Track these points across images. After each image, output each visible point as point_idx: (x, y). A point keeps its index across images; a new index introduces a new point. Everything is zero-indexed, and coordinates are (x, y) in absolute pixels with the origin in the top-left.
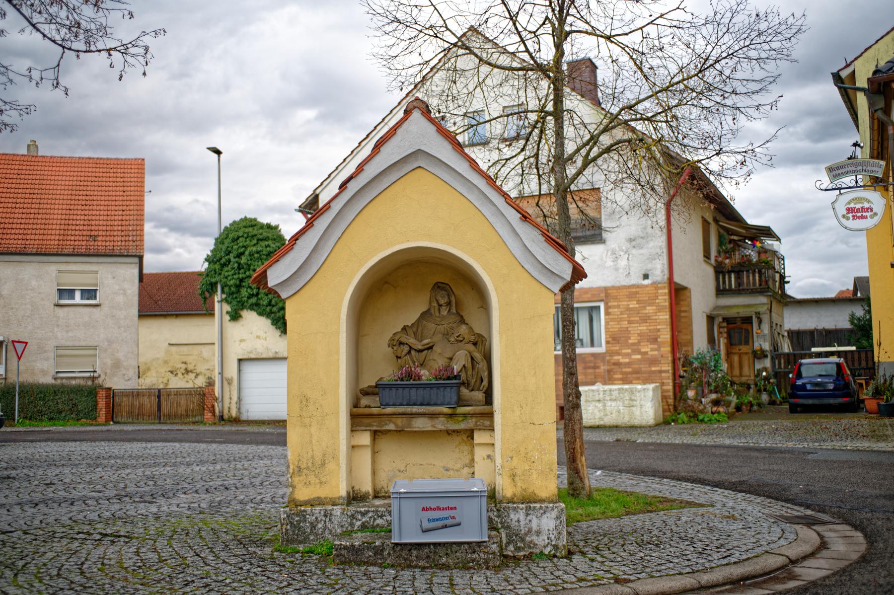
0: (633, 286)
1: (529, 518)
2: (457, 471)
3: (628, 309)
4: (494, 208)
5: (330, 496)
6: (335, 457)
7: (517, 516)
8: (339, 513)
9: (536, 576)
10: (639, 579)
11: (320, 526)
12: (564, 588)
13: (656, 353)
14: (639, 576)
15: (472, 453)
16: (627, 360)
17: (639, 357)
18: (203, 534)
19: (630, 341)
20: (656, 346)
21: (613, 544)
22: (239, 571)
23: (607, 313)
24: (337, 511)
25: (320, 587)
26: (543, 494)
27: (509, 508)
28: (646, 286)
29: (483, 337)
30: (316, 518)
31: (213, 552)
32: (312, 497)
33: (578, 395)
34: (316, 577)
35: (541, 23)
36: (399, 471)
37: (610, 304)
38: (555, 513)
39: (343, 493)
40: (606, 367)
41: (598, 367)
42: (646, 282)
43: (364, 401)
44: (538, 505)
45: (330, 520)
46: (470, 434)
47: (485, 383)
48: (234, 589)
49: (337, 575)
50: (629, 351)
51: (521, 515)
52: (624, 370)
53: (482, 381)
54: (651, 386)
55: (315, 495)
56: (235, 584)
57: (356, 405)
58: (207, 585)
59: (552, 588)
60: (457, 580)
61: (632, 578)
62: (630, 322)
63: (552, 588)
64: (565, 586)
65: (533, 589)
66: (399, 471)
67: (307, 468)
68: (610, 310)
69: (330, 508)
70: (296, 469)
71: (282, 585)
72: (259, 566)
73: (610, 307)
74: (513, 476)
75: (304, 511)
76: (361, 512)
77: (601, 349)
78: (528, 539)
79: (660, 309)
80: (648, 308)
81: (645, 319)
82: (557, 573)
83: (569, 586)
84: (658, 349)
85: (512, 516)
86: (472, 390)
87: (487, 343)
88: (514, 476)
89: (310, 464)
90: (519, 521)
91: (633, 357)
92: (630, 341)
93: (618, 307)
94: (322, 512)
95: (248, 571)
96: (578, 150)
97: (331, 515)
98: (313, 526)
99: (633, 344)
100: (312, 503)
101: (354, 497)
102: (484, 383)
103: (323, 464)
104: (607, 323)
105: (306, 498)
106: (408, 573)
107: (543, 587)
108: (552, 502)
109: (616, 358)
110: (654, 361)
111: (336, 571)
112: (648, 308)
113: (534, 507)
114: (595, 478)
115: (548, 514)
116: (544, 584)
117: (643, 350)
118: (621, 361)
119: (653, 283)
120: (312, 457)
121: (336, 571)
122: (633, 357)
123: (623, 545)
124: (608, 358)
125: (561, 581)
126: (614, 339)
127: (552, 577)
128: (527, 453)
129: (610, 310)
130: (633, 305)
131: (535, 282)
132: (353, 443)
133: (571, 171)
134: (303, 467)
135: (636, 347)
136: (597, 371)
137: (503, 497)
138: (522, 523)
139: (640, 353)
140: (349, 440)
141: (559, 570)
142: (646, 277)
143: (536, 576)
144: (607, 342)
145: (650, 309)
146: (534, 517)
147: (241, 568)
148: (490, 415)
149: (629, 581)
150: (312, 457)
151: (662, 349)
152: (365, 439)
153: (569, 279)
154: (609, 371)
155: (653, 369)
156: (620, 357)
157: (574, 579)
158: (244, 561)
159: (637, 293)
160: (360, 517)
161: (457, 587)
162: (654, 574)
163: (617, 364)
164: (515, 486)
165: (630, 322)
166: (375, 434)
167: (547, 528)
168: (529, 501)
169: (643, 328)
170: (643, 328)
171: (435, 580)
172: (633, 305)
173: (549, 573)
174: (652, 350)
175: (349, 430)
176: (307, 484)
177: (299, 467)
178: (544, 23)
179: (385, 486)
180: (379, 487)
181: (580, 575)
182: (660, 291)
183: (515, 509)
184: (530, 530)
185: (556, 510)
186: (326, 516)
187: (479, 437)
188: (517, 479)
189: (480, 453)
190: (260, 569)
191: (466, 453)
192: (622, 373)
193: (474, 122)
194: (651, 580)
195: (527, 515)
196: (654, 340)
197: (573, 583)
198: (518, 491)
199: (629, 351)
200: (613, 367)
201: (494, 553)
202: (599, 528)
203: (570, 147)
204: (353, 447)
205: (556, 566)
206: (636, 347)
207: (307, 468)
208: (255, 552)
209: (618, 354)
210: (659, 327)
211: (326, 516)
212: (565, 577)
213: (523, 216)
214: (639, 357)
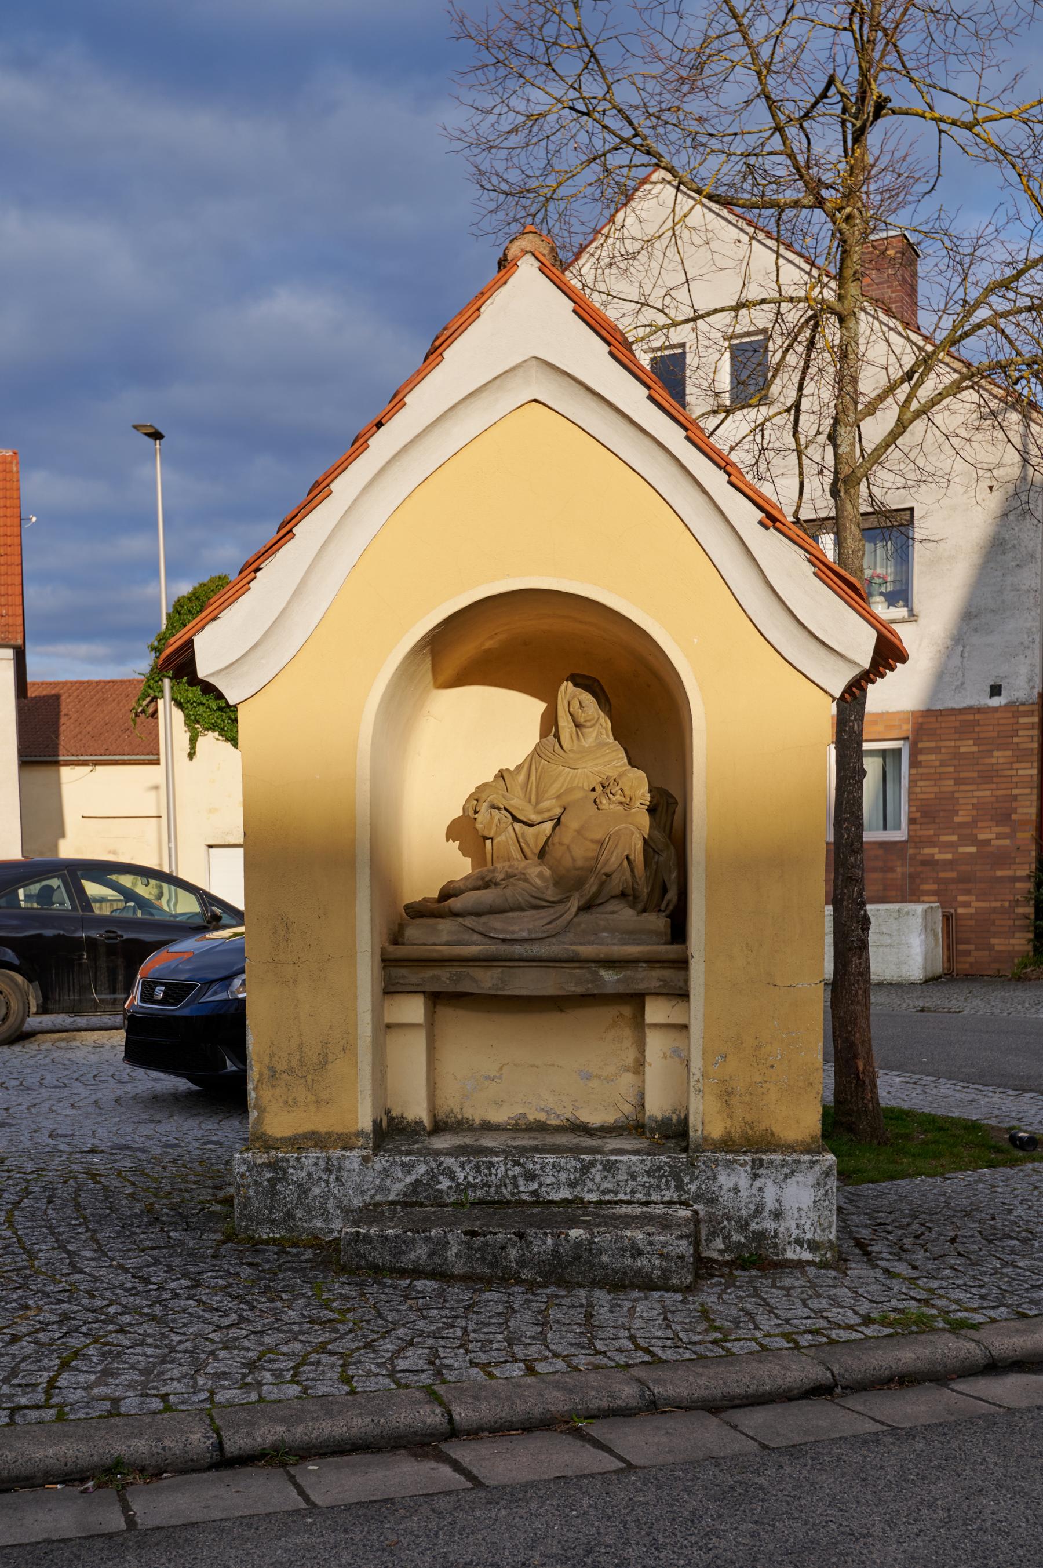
0: (969, 710)
1: (758, 1183)
2: (608, 1080)
3: (957, 755)
4: (701, 498)
5: (339, 1129)
6: (349, 1048)
7: (733, 1179)
8: (356, 1166)
9: (771, 1310)
10: (993, 1320)
11: (316, 1191)
12: (832, 1342)
13: (1007, 842)
14: (992, 1313)
15: (641, 1046)
16: (949, 856)
17: (973, 849)
18: (84, 1198)
19: (957, 819)
20: (1007, 830)
21: (933, 1235)
22: (141, 1287)
23: (913, 764)
24: (353, 1159)
25: (306, 1326)
26: (791, 1134)
27: (716, 1162)
28: (996, 709)
29: (671, 796)
30: (310, 1174)
31: (97, 1242)
32: (300, 1131)
33: (865, 923)
34: (302, 1301)
35: (818, 90)
36: (487, 1078)
37: (920, 745)
38: (811, 1178)
39: (366, 1123)
40: (907, 870)
41: (892, 870)
42: (996, 702)
43: (414, 931)
44: (778, 1157)
45: (337, 1179)
46: (637, 1000)
47: (672, 895)
48: (121, 1331)
49: (346, 1298)
50: (954, 838)
51: (741, 1178)
52: (942, 875)
53: (665, 890)
54: (919, 908)
55: (307, 1127)
56: (127, 1319)
57: (396, 938)
58: (65, 1317)
59: (805, 1340)
60: (603, 1313)
61: (978, 1318)
62: (958, 782)
63: (805, 1340)
64: (833, 1334)
65: (766, 1341)
66: (487, 1078)
67: (290, 1071)
68: (921, 758)
69: (337, 1153)
70: (267, 1073)
71: (226, 1322)
72: (184, 1275)
73: (921, 752)
74: (726, 1095)
75: (282, 1159)
76: (402, 1164)
77: (899, 835)
78: (754, 1226)
79: (1020, 756)
80: (995, 753)
81: (988, 776)
82: (814, 1303)
83: (844, 1335)
84: (1011, 836)
85: (722, 1179)
86: (644, 911)
87: (679, 810)
88: (729, 1094)
89: (295, 1063)
90: (736, 1190)
91: (961, 850)
92: (957, 819)
93: (936, 750)
94: (321, 1163)
95: (161, 1288)
96: (890, 389)
97: (340, 1169)
98: (303, 1190)
99: (961, 825)
100: (298, 1143)
101: (390, 1132)
102: (668, 897)
103: (324, 1063)
104: (912, 783)
105: (288, 1133)
106: (496, 1296)
107: (784, 1335)
108: (808, 1151)
109: (927, 851)
110: (1001, 859)
111: (346, 1290)
112: (995, 753)
113: (771, 1162)
114: (892, 1090)
115: (799, 1177)
116: (787, 1328)
117: (981, 837)
118: (937, 857)
119: (1011, 705)
120: (300, 1047)
121: (346, 1290)
122: (961, 850)
123: (953, 1240)
124: (911, 851)
125: (824, 1324)
126: (925, 814)
127: (806, 1312)
128: (758, 1047)
129: (921, 758)
130: (967, 747)
131: (814, 641)
132: (387, 1020)
133: (874, 429)
134: (280, 1068)
135: (968, 831)
136: (890, 875)
137: (705, 1139)
138: (744, 1193)
139: (975, 842)
140: (377, 1012)
141: (819, 1296)
142: (996, 690)
143: (771, 1310)
144: (912, 821)
145: (1000, 756)
146: (769, 1183)
147: (146, 1281)
148: (682, 964)
149: (975, 1327)
150: (300, 1047)
151: (1019, 835)
152: (412, 1010)
153: (867, 666)
154: (912, 877)
155: (999, 873)
156: (936, 850)
157: (854, 1320)
158: (156, 1262)
159: (977, 723)
160: (400, 1175)
161: (600, 1334)
162: (1025, 1309)
163: (930, 863)
164: (730, 1116)
165: (958, 782)
166: (436, 999)
167: (795, 1206)
168: (755, 1147)
169: (984, 793)
170: (984, 793)
171: (554, 1313)
172: (967, 747)
173: (799, 1304)
174: (999, 836)
175: (379, 991)
176: (290, 1104)
177: (272, 1069)
178: (824, 95)
179: (457, 1110)
180: (441, 1114)
181: (864, 1307)
182: (1022, 720)
183: (729, 1164)
184: (758, 1211)
185: (817, 1168)
186: (328, 1170)
187: (656, 1012)
188: (734, 1101)
189: (656, 1044)
190: (184, 1282)
191: (627, 1043)
192: (938, 881)
193: (661, 320)
194: (1020, 1325)
195: (755, 1176)
196: (1004, 816)
197: (850, 1327)
198: (737, 1128)
199: (954, 838)
200: (919, 869)
201: (681, 1257)
202: (902, 1198)
203: (870, 383)
204: (389, 1026)
205: (813, 1286)
206: (968, 831)
207: (290, 1071)
208: (182, 1243)
209: (932, 844)
210: (1015, 792)
211: (328, 1170)
212: (834, 1313)
213: (770, 516)
214: (973, 849)
